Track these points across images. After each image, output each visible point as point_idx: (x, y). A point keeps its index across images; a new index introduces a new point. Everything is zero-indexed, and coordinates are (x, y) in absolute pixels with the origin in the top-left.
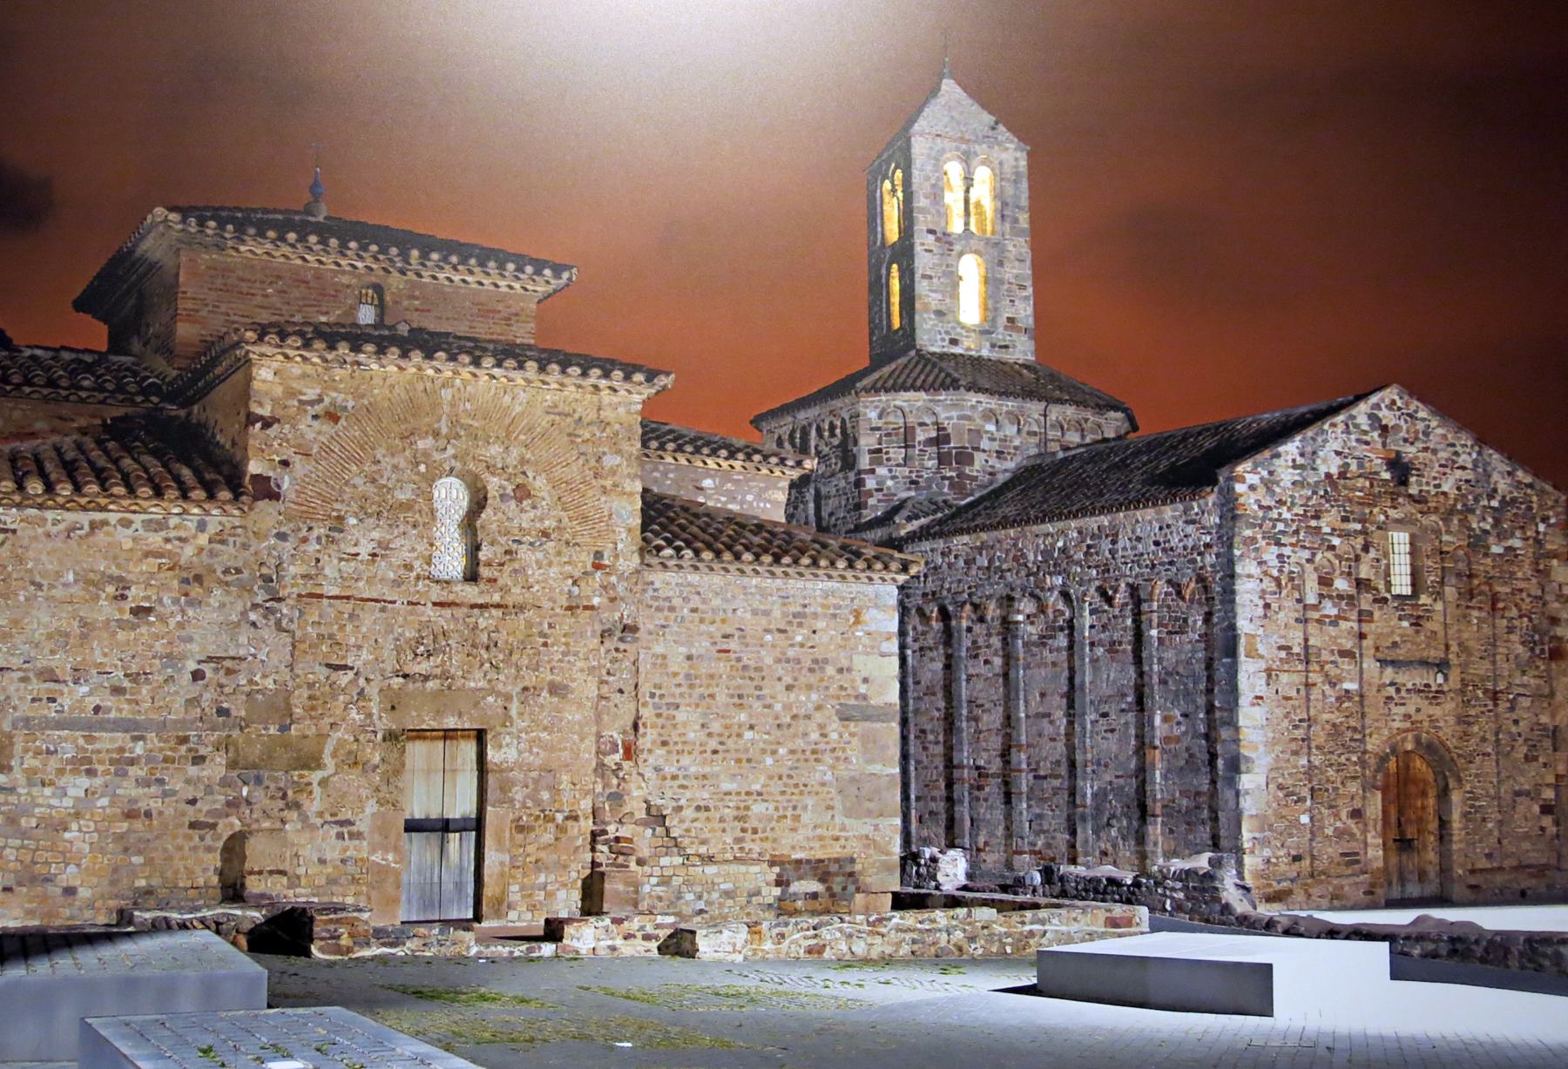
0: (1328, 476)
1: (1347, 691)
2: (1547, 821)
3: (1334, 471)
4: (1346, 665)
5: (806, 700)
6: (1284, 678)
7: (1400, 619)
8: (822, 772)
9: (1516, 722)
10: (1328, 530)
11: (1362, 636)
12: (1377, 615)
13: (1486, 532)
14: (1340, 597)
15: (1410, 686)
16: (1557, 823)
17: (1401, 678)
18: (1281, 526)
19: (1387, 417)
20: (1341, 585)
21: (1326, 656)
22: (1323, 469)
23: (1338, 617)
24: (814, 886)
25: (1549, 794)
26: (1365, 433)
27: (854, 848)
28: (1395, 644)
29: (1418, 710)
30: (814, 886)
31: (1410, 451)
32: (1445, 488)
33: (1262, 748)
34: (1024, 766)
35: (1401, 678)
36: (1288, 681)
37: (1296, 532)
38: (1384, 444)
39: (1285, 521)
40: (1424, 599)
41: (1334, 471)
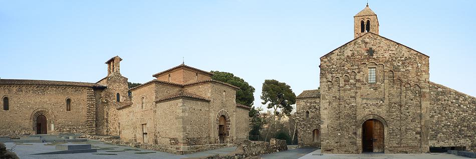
0: (348, 56)
1: (353, 106)
2: (418, 136)
3: (350, 55)
4: (352, 100)
5: (172, 117)
6: (334, 103)
7: (370, 88)
8: (174, 127)
9: (409, 113)
10: (347, 69)
11: (356, 93)
12: (362, 88)
13: (399, 66)
14: (351, 84)
15: (371, 104)
16: (421, 136)
17: (368, 102)
18: (333, 70)
19: (367, 40)
20: (352, 81)
21: (346, 98)
22: (346, 55)
23: (350, 89)
24: (174, 141)
25: (419, 129)
26: (360, 45)
27: (177, 137)
28: (368, 94)
29: (374, 110)
30: (174, 141)
31: (374, 48)
32: (386, 56)
33: (326, 119)
34: (338, 122)
35: (368, 102)
36: (335, 104)
37: (337, 71)
38: (366, 47)
39: (334, 68)
40: (378, 83)
41: (350, 55)
